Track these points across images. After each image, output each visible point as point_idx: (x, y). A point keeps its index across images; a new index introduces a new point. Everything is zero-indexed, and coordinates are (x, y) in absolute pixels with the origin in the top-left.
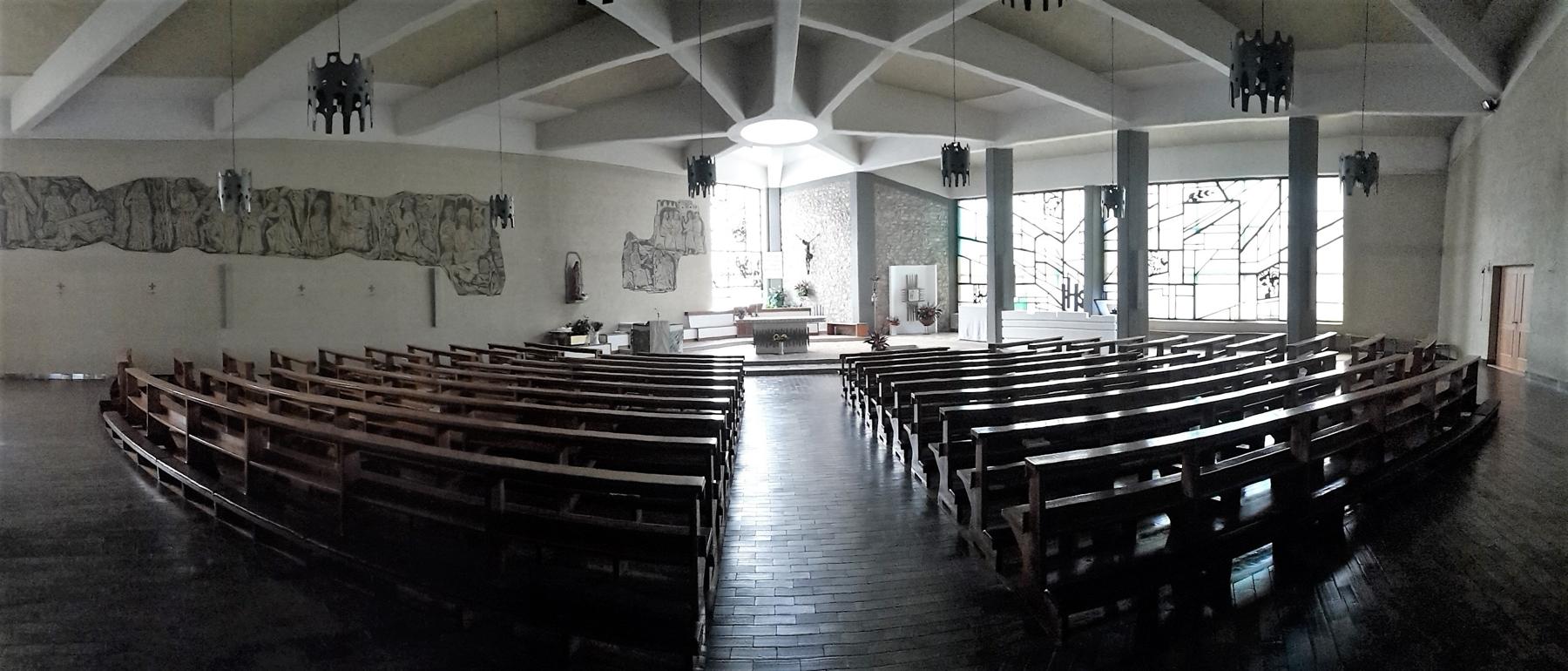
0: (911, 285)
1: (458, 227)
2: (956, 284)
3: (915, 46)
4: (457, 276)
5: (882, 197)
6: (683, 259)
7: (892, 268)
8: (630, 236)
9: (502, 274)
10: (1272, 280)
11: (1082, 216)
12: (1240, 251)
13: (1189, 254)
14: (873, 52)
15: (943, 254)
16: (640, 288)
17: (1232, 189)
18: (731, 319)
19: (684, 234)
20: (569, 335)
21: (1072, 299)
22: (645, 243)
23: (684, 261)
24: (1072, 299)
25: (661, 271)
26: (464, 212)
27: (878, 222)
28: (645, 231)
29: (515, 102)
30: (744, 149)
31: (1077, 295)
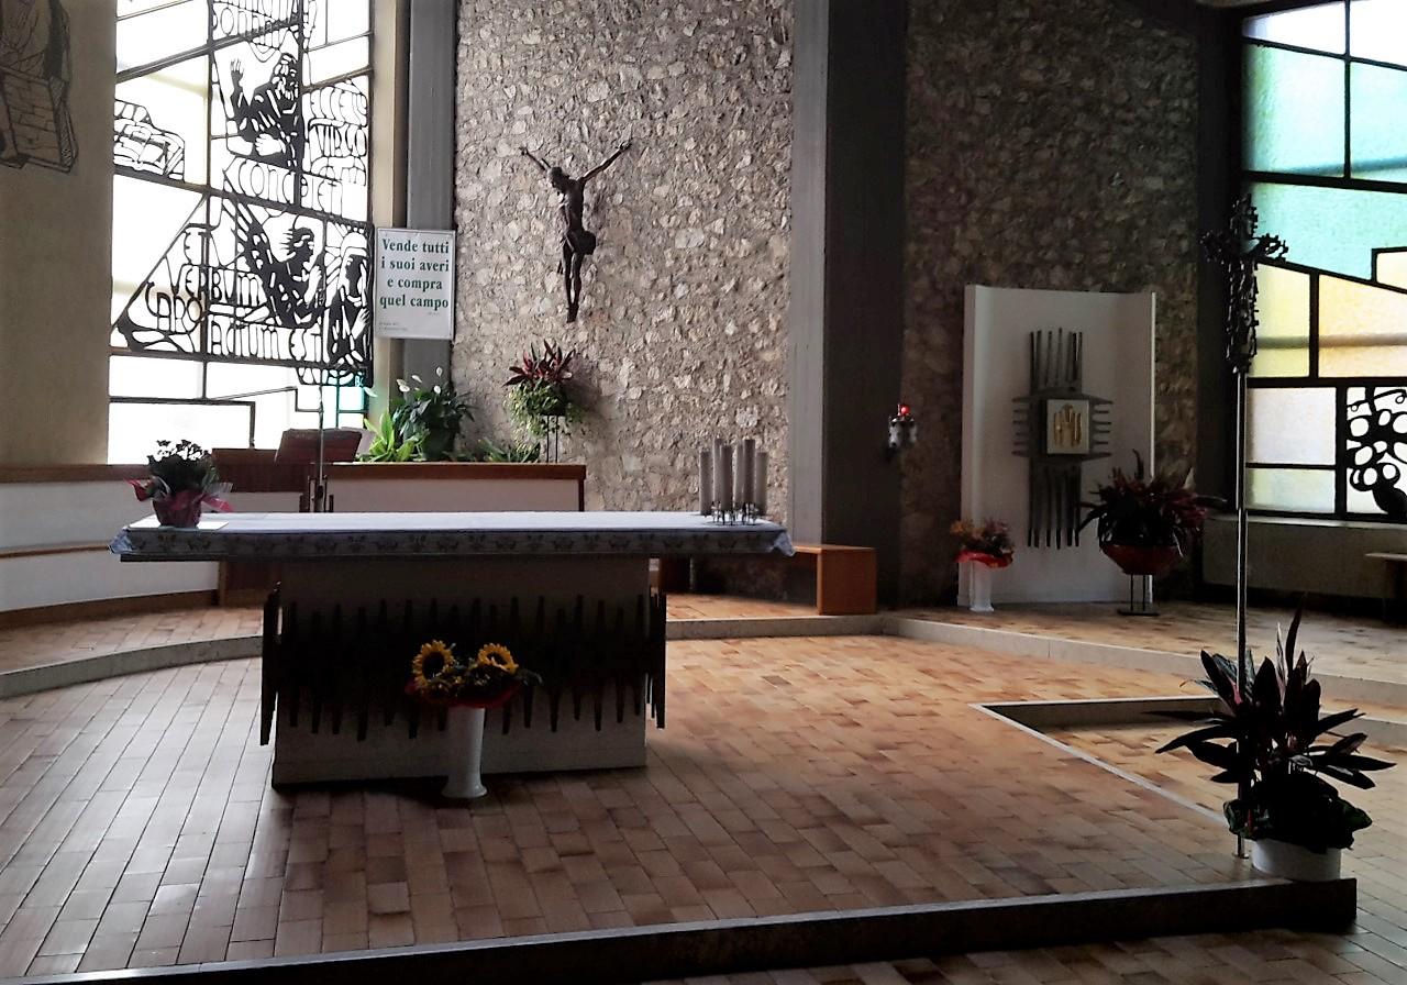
0: (1049, 376)
7: (982, 301)
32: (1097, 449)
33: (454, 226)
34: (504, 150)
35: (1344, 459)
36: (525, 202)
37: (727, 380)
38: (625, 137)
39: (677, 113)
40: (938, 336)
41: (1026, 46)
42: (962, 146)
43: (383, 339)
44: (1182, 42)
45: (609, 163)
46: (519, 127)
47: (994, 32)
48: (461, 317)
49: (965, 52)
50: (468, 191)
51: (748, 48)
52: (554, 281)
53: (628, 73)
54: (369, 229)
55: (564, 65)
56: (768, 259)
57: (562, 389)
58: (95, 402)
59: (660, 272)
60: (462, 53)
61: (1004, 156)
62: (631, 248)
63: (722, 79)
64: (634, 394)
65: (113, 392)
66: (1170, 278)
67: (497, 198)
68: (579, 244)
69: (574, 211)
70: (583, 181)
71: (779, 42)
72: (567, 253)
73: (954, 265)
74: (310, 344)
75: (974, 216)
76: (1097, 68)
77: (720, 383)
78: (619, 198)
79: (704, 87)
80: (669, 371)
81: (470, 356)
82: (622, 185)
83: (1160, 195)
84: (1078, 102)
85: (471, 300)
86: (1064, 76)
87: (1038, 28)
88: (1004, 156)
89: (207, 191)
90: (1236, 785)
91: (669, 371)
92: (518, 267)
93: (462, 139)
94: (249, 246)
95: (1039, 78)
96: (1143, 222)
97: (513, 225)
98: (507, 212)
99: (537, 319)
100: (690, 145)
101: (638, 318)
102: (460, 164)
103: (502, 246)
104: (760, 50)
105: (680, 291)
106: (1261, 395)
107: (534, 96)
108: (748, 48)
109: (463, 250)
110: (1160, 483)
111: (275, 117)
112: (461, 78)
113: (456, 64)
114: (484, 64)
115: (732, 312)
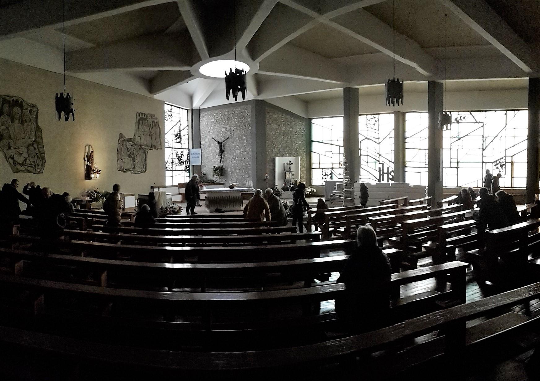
0: (287, 167)
1: (12, 121)
2: (310, 169)
3: (331, 20)
4: (12, 158)
5: (271, 116)
8: (121, 136)
9: (44, 158)
10: (502, 166)
11: (393, 127)
12: (483, 150)
13: (454, 151)
14: (309, 18)
16: (127, 170)
17: (479, 116)
19: (151, 136)
20: (90, 201)
21: (385, 176)
22: (130, 140)
23: (151, 153)
24: (385, 176)
25: (139, 159)
26: (16, 110)
27: (268, 132)
28: (130, 133)
29: (51, 32)
31: (388, 173)
35: (323, 178)
36: (212, 145)
40: (271, 164)
46: (211, 134)
52: (218, 157)
53: (228, 128)
54: (189, 149)
57: (220, 171)
58: (164, 177)
67: (208, 144)
68: (222, 152)
69: (220, 147)
73: (273, 155)
74: (183, 167)
80: (236, 170)
90: (334, 300)
91: (236, 170)
93: (201, 135)
110: (306, 204)
111: (178, 136)
115: (244, 162)
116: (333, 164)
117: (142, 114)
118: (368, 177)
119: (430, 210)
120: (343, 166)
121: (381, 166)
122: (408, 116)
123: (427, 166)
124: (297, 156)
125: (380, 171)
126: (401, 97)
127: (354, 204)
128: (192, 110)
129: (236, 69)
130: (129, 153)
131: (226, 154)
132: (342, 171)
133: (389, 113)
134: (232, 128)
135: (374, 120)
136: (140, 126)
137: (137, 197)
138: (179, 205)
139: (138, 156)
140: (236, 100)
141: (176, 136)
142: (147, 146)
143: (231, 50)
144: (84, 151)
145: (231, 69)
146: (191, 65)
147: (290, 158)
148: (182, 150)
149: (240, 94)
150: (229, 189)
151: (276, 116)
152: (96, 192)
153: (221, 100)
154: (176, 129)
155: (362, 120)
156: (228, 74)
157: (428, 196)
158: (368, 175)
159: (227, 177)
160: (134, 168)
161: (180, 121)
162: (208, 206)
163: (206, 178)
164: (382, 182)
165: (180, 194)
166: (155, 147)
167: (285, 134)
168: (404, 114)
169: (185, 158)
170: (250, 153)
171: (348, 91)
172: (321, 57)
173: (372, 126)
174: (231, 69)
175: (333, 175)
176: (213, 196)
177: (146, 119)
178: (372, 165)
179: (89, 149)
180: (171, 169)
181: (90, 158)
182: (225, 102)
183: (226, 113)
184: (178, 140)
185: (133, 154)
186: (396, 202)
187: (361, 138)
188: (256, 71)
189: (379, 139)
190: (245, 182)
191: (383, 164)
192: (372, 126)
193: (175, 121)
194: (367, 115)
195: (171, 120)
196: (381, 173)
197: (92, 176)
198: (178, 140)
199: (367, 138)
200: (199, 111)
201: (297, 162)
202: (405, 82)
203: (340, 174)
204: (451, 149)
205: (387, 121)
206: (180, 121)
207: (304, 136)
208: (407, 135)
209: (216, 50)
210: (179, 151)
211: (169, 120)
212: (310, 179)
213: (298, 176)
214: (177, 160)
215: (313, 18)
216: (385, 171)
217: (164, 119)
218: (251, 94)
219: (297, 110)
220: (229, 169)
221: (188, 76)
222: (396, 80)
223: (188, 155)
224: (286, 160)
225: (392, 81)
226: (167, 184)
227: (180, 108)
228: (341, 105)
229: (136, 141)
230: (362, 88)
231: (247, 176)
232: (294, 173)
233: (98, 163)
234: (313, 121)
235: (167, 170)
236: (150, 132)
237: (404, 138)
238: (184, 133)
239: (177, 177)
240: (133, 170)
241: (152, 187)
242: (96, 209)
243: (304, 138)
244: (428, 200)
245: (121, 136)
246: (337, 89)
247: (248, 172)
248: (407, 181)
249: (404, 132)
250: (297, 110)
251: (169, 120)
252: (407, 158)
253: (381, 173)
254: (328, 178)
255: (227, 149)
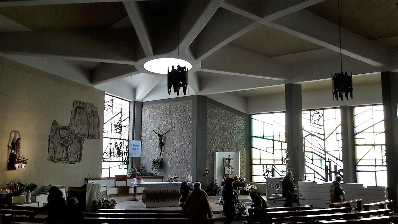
0: (226, 163)
2: (250, 164)
6: (86, 141)
7: (217, 153)
8: (55, 123)
15: (243, 145)
16: (59, 160)
18: (112, 183)
19: (88, 125)
20: (10, 196)
21: (333, 175)
22: (64, 128)
23: (87, 143)
25: (72, 149)
28: (65, 121)
30: (142, 74)
31: (336, 172)
32: (232, 173)
33: (141, 140)
34: (149, 129)
35: (264, 175)
36: (153, 137)
37: (183, 165)
38: (169, 130)
39: (176, 127)
40: (211, 159)
41: (222, 120)
42: (214, 134)
43: (130, 157)
44: (243, 119)
45: (166, 133)
46: (152, 126)
47: (218, 118)
48: (142, 153)
49: (214, 121)
50: (143, 135)
51: (186, 120)
54: (128, 140)
55: (159, 118)
56: (189, 148)
57: (160, 164)
58: (100, 169)
59: (174, 149)
60: (143, 114)
61: (220, 134)
62: (169, 145)
63: (182, 123)
64: (170, 166)
65: (102, 167)
66: (242, 150)
67: (149, 136)
68: (162, 144)
69: (161, 140)
70: (162, 135)
71: (191, 120)
72: (160, 146)
73: (213, 149)
74: (121, 159)
75: (216, 143)
76: (232, 122)
77: (182, 165)
78: (168, 138)
79: (180, 124)
80: (175, 163)
81: (143, 160)
82: (168, 136)
83: (240, 139)
84: (229, 127)
85: (144, 151)
86: (228, 124)
87: (224, 118)
88: (220, 134)
89: (111, 138)
91: (175, 163)
92: (152, 146)
93: (143, 127)
94: (116, 145)
95: (224, 124)
96: (238, 143)
97: (151, 140)
98: (150, 138)
99: (155, 154)
100: (178, 132)
101: (170, 155)
102: (142, 131)
103: (149, 143)
104: (188, 120)
105: (177, 152)
106: (254, 166)
107: (154, 122)
108: (186, 120)
109: (142, 143)
111: (119, 127)
112: (142, 118)
113: (142, 116)
114: (146, 116)
115: (184, 155)
116: (274, 160)
117: (80, 102)
118: (313, 175)
119: (392, 216)
120: (285, 163)
121: (328, 164)
122: (357, 110)
123: (385, 164)
124: (237, 151)
125: (326, 169)
126: (351, 90)
127: (299, 205)
128: (135, 102)
129: (178, 66)
130: (62, 142)
131: (166, 147)
132: (284, 168)
133: (335, 108)
134: (173, 121)
135: (318, 115)
136: (77, 115)
137: (67, 189)
138: (113, 198)
139: (72, 145)
140: (178, 94)
141: (116, 127)
142: (84, 135)
143: (176, 49)
144: (8, 138)
145: (173, 66)
146: (136, 60)
147: (228, 154)
148: (122, 141)
149: (181, 89)
150: (167, 183)
151: (216, 111)
152: (19, 184)
153: (163, 94)
154: (117, 120)
155: (305, 115)
156: (170, 71)
157: (389, 198)
158: (314, 173)
159: (166, 170)
160: (67, 158)
161: (121, 112)
162: (145, 201)
163: (145, 171)
164: (330, 182)
165: (116, 187)
166: (93, 137)
167: (225, 129)
168: (352, 108)
169: (124, 150)
170: (190, 147)
171: (289, 88)
172: (260, 56)
173: (316, 122)
174: (173, 66)
175: (275, 173)
176: (150, 190)
177: (83, 108)
178: (318, 163)
179: (15, 136)
180: (108, 160)
181: (15, 145)
182: (167, 96)
183: (168, 107)
184: (118, 131)
185: (67, 142)
186: (348, 205)
187: (304, 134)
188: (199, 68)
189: (324, 135)
190: (184, 176)
191: (330, 162)
192: (316, 122)
193: (116, 110)
194: (310, 110)
195: (111, 110)
196: (329, 171)
197: (17, 166)
198: (118, 131)
199: (310, 134)
200: (142, 104)
201: (236, 158)
202: (353, 76)
203: (283, 171)
204: (109, 168)
205: (333, 117)
206: (121, 112)
207: (244, 132)
208: (357, 130)
209: (160, 49)
210: (119, 142)
211: (109, 111)
212: (250, 175)
213: (237, 171)
214: (116, 151)
215: (254, 21)
216: (333, 170)
217: (103, 109)
218: (192, 90)
219: (237, 106)
220: (169, 162)
221: (132, 70)
222: (344, 74)
223: (128, 147)
224: (226, 155)
225: (339, 74)
226: (103, 176)
227: (122, 99)
228: (283, 101)
229: (72, 129)
230: (305, 84)
231: (186, 170)
232: (234, 169)
233: (25, 151)
234: (253, 117)
235: (104, 161)
236: (88, 121)
237: (353, 134)
238: (125, 124)
239: (114, 168)
240: (66, 160)
241: (86, 179)
242: (19, 203)
243: (244, 133)
244: (388, 203)
245: (55, 123)
246: (279, 86)
247: (187, 166)
248: (360, 182)
249: (353, 127)
250: (237, 106)
251: (109, 111)
252: (359, 156)
253: (329, 171)
254: (270, 176)
255: (168, 142)
